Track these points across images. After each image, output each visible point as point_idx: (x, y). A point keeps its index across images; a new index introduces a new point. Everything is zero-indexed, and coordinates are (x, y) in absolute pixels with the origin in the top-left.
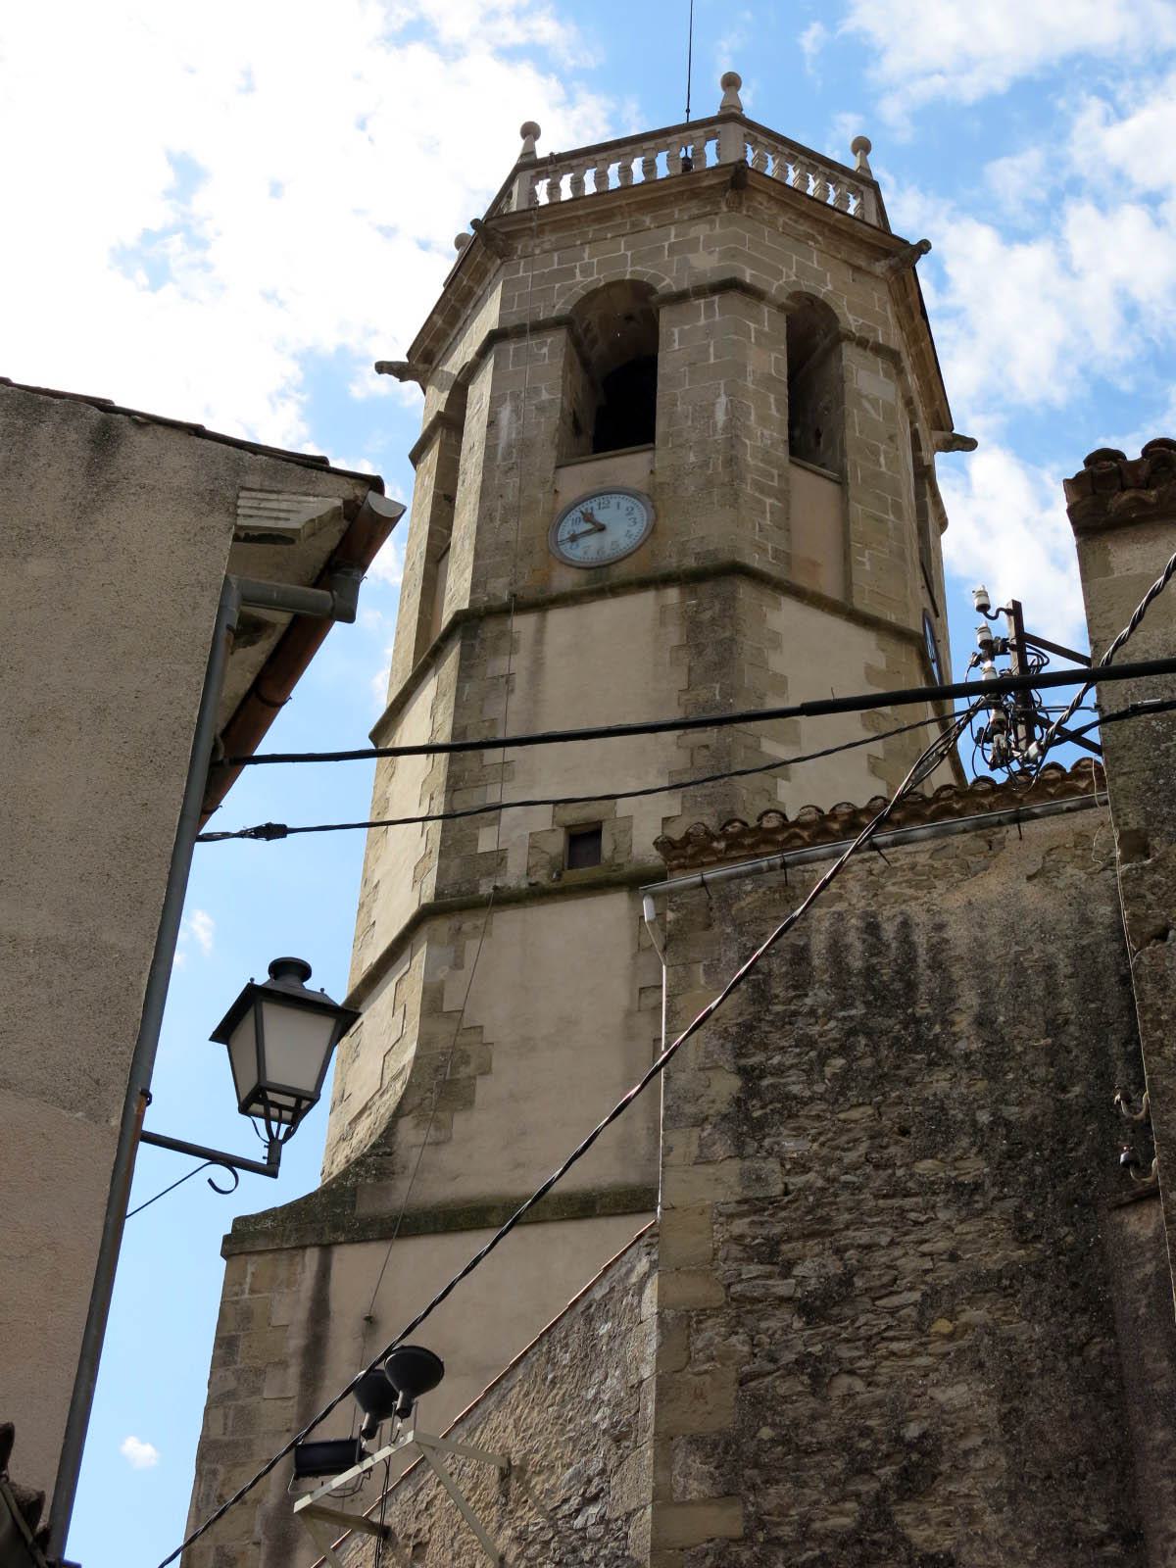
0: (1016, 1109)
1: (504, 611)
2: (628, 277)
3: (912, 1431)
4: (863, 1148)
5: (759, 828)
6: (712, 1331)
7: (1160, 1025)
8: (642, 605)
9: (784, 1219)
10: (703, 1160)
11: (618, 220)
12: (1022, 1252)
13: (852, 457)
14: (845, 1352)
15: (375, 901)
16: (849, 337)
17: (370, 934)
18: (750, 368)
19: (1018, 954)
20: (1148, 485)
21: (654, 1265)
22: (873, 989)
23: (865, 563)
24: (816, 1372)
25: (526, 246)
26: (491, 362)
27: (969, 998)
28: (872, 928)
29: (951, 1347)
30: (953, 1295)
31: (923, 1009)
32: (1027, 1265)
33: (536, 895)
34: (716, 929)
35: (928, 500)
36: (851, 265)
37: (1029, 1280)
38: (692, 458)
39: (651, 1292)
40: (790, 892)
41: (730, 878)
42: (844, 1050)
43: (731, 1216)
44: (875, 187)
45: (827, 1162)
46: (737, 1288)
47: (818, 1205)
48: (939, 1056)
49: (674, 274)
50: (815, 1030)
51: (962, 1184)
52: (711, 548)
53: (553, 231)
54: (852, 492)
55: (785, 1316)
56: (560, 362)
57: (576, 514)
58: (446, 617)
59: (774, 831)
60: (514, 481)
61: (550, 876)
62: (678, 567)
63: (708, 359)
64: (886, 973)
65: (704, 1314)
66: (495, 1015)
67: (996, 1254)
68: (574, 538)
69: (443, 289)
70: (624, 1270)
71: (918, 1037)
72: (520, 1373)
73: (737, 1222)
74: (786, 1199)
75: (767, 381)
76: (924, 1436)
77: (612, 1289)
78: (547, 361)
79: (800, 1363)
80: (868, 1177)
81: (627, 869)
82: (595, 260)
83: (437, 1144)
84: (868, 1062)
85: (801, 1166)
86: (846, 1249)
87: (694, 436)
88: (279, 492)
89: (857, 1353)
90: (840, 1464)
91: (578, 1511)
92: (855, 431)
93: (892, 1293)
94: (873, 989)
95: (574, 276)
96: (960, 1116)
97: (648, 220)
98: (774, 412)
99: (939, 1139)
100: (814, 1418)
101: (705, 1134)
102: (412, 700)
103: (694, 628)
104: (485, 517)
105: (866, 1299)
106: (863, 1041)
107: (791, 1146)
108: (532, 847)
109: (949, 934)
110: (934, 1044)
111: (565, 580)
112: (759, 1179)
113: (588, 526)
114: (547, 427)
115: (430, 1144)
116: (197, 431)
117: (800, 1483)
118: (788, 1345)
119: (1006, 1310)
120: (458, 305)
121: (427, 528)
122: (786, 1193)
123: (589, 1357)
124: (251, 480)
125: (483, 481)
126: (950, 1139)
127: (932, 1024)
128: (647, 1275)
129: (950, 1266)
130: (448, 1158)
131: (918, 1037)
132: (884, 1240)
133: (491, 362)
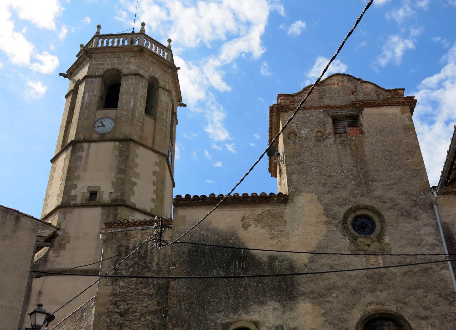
0: (161, 281)
1: (82, 142)
2: (116, 68)
4: (134, 286)
5: (123, 222)
6: (104, 317)
7: (172, 296)
8: (110, 145)
9: (119, 298)
10: (106, 285)
11: (116, 54)
12: (158, 307)
13: (158, 114)
14: (126, 323)
15: (48, 199)
16: (161, 87)
17: (47, 206)
19: (165, 252)
20: (185, 201)
21: (95, 304)
22: (139, 255)
23: (158, 138)
25: (95, 56)
26: (84, 83)
27: (156, 259)
29: (144, 323)
30: (146, 314)
31: (148, 261)
32: (159, 310)
33: (82, 206)
35: (174, 119)
36: (163, 70)
37: (159, 312)
38: (125, 113)
39: (94, 309)
40: (127, 235)
41: (116, 232)
42: (133, 267)
44: (171, 51)
45: (127, 288)
46: (109, 310)
47: (125, 296)
48: (149, 270)
49: (126, 69)
50: (128, 262)
51: (150, 294)
52: (126, 134)
55: (117, 315)
56: (99, 85)
57: (99, 122)
58: (69, 142)
59: (126, 223)
61: (86, 202)
62: (119, 137)
63: (130, 90)
64: (142, 253)
65: (103, 314)
67: (154, 307)
68: (98, 127)
69: (76, 59)
70: (89, 304)
71: (146, 266)
72: (69, 319)
73: (111, 297)
74: (120, 294)
77: (87, 307)
78: (97, 85)
81: (102, 203)
82: (110, 62)
83: (57, 257)
84: (137, 270)
85: (123, 288)
86: (129, 304)
88: (44, 229)
89: (128, 323)
92: (159, 109)
93: (136, 313)
94: (139, 255)
95: (104, 65)
96: (151, 282)
97: (122, 55)
98: (143, 104)
99: (147, 285)
101: (107, 280)
102: (60, 155)
103: (121, 151)
104: (80, 119)
105: (131, 314)
106: (136, 265)
107: (122, 284)
108: (83, 195)
110: (148, 267)
111: (95, 136)
112: (115, 290)
113: (102, 125)
115: (56, 257)
116: (32, 217)
118: (116, 321)
119: (154, 317)
120: (79, 64)
121: (67, 115)
122: (120, 293)
123: (82, 319)
125: (80, 110)
126: (149, 285)
127: (149, 263)
128: (93, 306)
129: (146, 309)
130: (59, 260)
131: (146, 266)
133: (84, 83)
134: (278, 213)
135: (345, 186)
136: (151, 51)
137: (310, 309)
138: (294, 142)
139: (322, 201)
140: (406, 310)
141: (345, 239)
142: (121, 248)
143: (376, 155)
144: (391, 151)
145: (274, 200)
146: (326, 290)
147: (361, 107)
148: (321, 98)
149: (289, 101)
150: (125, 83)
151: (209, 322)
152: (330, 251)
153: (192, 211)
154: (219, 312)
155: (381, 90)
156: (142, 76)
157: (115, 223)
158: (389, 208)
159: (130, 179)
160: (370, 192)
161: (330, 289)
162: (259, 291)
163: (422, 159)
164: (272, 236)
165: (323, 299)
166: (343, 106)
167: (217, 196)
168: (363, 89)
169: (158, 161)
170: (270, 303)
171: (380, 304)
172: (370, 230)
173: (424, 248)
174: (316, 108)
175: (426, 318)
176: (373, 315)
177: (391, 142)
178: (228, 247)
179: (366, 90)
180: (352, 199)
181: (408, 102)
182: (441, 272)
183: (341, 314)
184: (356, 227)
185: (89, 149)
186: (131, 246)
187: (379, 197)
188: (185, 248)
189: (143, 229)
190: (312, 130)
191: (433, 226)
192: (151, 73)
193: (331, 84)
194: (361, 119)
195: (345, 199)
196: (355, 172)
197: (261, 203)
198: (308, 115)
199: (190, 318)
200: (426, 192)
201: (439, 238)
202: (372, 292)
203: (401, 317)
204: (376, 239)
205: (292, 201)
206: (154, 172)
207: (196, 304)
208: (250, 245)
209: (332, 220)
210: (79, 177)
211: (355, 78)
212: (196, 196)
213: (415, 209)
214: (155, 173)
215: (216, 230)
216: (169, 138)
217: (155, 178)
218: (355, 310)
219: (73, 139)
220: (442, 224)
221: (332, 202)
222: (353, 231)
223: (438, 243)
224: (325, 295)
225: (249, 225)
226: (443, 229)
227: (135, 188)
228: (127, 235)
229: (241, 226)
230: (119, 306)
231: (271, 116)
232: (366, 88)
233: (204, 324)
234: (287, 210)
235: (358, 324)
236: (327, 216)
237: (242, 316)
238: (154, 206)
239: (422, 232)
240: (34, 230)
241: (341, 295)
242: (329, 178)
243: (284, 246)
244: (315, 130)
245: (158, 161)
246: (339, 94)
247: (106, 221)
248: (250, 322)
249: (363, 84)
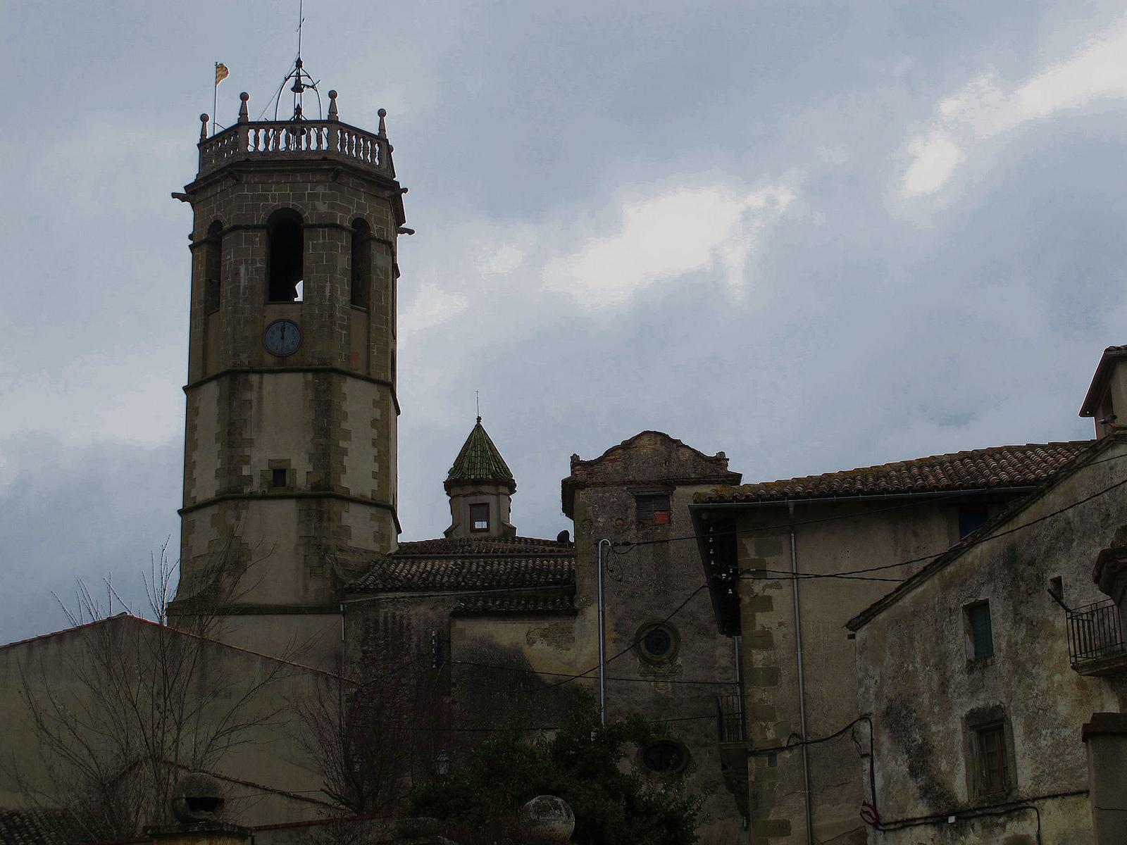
8: (296, 380)
28: (394, 617)
33: (264, 497)
109: (411, 621)
139: (614, 613)
150: (311, 243)
159: (338, 445)
168: (678, 457)
174: (618, 484)
175: (706, 745)
185: (261, 383)
191: (730, 646)
192: (355, 212)
201: (734, 659)
206: (373, 420)
208: (536, 666)
210: (251, 442)
223: (731, 666)
225: (535, 642)
227: (346, 460)
238: (376, 486)
239: (717, 653)
244: (614, 517)
245: (377, 397)
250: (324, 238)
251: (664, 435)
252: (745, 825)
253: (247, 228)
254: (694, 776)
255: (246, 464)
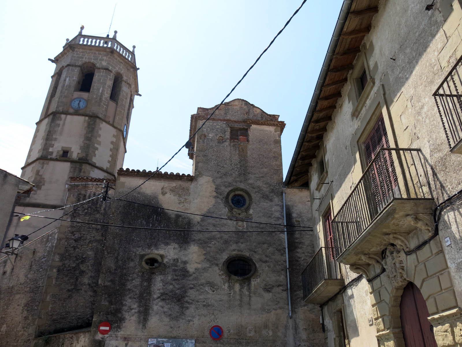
3: (84, 257)
6: (63, 241)
7: (109, 234)
8: (81, 119)
14: (79, 246)
18: (107, 84)
22: (93, 202)
23: (117, 118)
24: (75, 248)
27: (104, 206)
33: (56, 160)
34: (75, 190)
42: (87, 209)
43: (69, 227)
46: (67, 237)
48: (98, 212)
53: (82, 49)
54: (118, 107)
56: (78, 73)
60: (67, 91)
66: (46, 177)
69: (61, 50)
75: (109, 86)
76: (85, 257)
79: (73, 247)
80: (86, 226)
81: (71, 159)
84: (90, 212)
87: (96, 93)
90: (75, 259)
91: (42, 259)
94: (93, 202)
95: (83, 58)
100: (73, 253)
114: (74, 84)
117: (70, 261)
118: (72, 244)
124: (21, 183)
132: (86, 234)
134: (186, 187)
135: (231, 174)
136: (119, 53)
137: (197, 250)
138: (204, 142)
139: (215, 182)
140: (255, 256)
141: (226, 209)
142: (80, 196)
143: (254, 157)
144: (264, 155)
145: (184, 178)
146: (208, 239)
147: (250, 124)
148: (225, 114)
149: (204, 113)
151: (132, 252)
152: (215, 215)
153: (130, 179)
154: (139, 247)
155: (264, 114)
156: (111, 71)
157: (78, 178)
158: (256, 192)
159: (94, 146)
160: (246, 180)
161: (211, 239)
162: (166, 236)
163: (282, 163)
164: (180, 202)
165: (206, 245)
166: (239, 121)
167: (147, 171)
168: (253, 112)
169: (116, 134)
170: (172, 244)
171: (240, 251)
172: (242, 204)
173: (273, 219)
175: (266, 262)
176: (234, 257)
177: (265, 150)
178: (150, 206)
179: (255, 113)
180: (234, 184)
181: (280, 125)
182: (280, 235)
183: (215, 255)
184: (234, 201)
186: (88, 195)
187: (251, 184)
188: (122, 204)
189: (97, 184)
190: (216, 135)
191: (280, 206)
193: (234, 105)
194: (249, 132)
195: (230, 183)
196: (239, 166)
197: (176, 179)
198: (215, 124)
199: (119, 249)
200: (280, 184)
201: (283, 214)
202: (237, 243)
203: (251, 260)
204: (244, 210)
205: (196, 180)
207: (125, 241)
208: (165, 206)
209: (219, 196)
210: (56, 139)
211: (249, 103)
212: (133, 170)
213: (271, 194)
214: (112, 143)
215: (144, 194)
216: (126, 119)
217: (112, 146)
218: (224, 253)
219: (54, 110)
220: (286, 205)
221: (222, 184)
222: (231, 204)
223: (281, 217)
224: (207, 242)
225: (166, 193)
226: (286, 209)
227: (97, 152)
228: (85, 187)
229: (161, 193)
230: (74, 235)
231: (191, 121)
232: (256, 111)
233: (128, 254)
234: (192, 186)
235: (224, 262)
236: (217, 193)
237: (154, 251)
239: (273, 209)
240: (17, 185)
241: (217, 243)
242: (222, 168)
243: (187, 209)
244: (218, 135)
245: (116, 134)
246: (237, 112)
247: (71, 176)
248: (158, 255)
249: (254, 108)
250: (103, 73)
251: (245, 101)
252: (290, 315)
253: (73, 66)
254: (258, 280)
255: (52, 147)
